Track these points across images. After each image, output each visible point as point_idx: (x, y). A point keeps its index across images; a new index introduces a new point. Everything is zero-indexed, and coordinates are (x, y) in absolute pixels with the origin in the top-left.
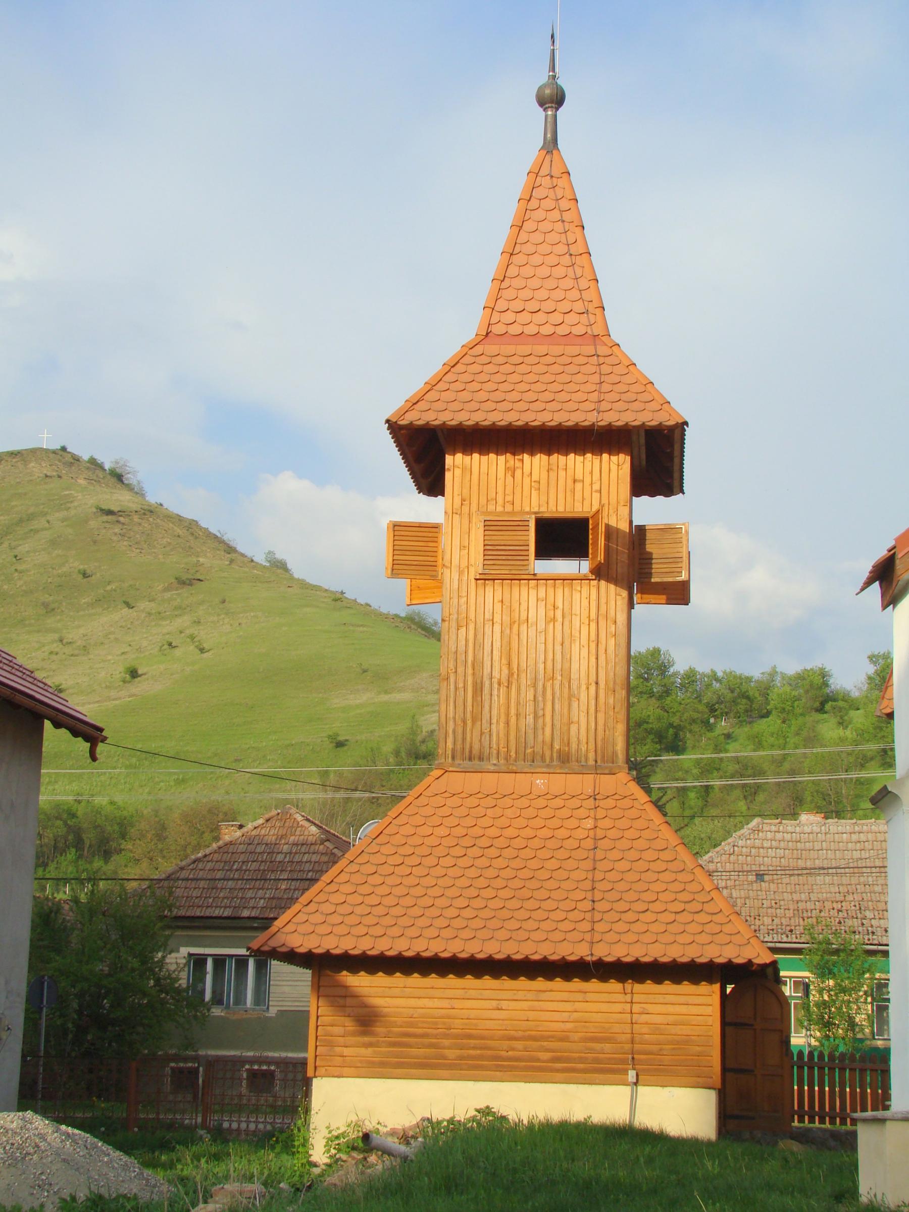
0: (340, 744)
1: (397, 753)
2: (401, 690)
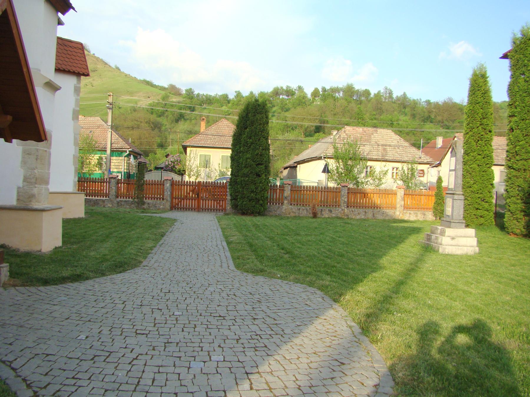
0: (120, 108)
1: (131, 110)
2: (136, 96)
